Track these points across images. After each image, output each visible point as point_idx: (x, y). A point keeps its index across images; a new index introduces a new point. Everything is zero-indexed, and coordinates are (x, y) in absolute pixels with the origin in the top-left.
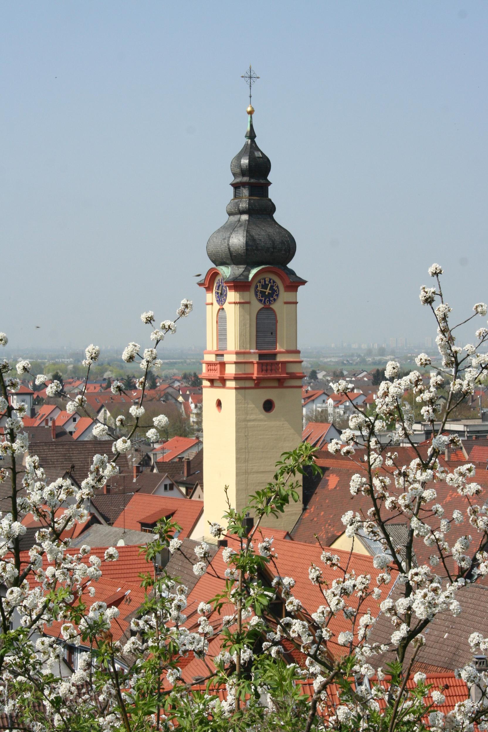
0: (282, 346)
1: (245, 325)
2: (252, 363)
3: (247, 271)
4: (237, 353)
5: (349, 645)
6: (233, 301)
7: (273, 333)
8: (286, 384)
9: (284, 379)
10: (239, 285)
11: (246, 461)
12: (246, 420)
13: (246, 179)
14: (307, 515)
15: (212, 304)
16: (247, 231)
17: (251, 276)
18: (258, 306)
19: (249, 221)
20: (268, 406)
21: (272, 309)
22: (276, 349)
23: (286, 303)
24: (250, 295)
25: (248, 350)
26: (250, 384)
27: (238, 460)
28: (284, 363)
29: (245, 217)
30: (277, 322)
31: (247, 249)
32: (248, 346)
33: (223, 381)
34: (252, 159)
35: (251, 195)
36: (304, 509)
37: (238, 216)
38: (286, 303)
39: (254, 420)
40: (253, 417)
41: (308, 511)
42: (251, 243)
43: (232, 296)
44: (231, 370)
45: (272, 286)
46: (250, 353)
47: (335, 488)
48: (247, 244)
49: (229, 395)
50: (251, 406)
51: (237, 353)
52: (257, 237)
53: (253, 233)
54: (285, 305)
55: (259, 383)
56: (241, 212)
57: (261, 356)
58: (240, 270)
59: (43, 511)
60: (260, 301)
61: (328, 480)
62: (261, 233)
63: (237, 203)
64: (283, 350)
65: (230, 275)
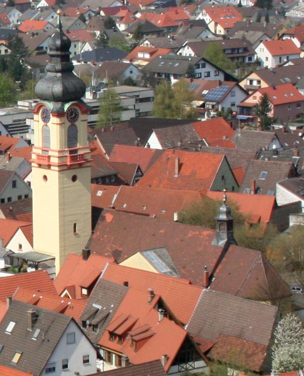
0: (80, 144)
1: (62, 135)
2: (66, 156)
3: (63, 106)
4: (59, 152)
5: (275, 137)
6: (56, 123)
7: (76, 138)
8: (83, 166)
9: (83, 163)
10: (59, 114)
11: (64, 209)
12: (64, 188)
13: (59, 53)
14: (94, 236)
15: (38, 121)
16: (63, 84)
17: (66, 109)
18: (68, 124)
19: (62, 77)
20: (74, 178)
21: (75, 125)
22: (77, 146)
23: (82, 121)
24: (65, 119)
25: (63, 149)
26: (65, 168)
27: (60, 209)
28: (82, 155)
29: (59, 75)
30: (77, 131)
31: (63, 95)
32: (64, 147)
33: (49, 167)
34: (62, 41)
35: (62, 61)
36: (93, 233)
37: (55, 74)
38: (82, 121)
39: (68, 187)
40: (66, 186)
41: (95, 234)
42: (66, 91)
43: (54, 120)
44: (55, 160)
45: (75, 113)
46: (64, 151)
47: (111, 222)
48: (63, 91)
49: (54, 175)
50: (66, 179)
51: (59, 152)
52: (67, 86)
53: (66, 84)
54: (82, 122)
55: (70, 167)
56: (57, 72)
57: (71, 152)
58: (59, 105)
59: (247, 238)
60: (70, 121)
61: (105, 217)
62: (70, 84)
63: (54, 66)
64: (81, 147)
65: (53, 108)
